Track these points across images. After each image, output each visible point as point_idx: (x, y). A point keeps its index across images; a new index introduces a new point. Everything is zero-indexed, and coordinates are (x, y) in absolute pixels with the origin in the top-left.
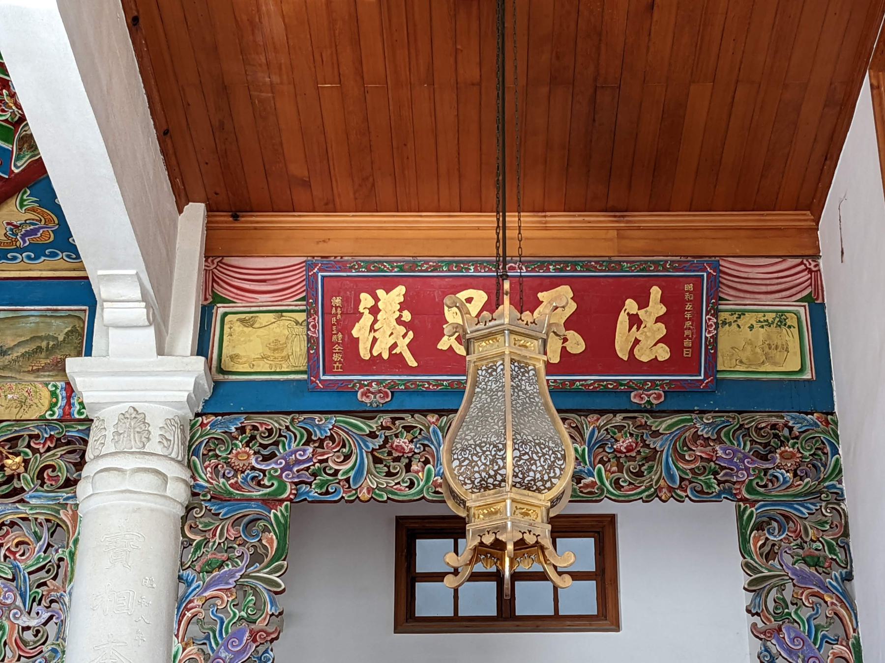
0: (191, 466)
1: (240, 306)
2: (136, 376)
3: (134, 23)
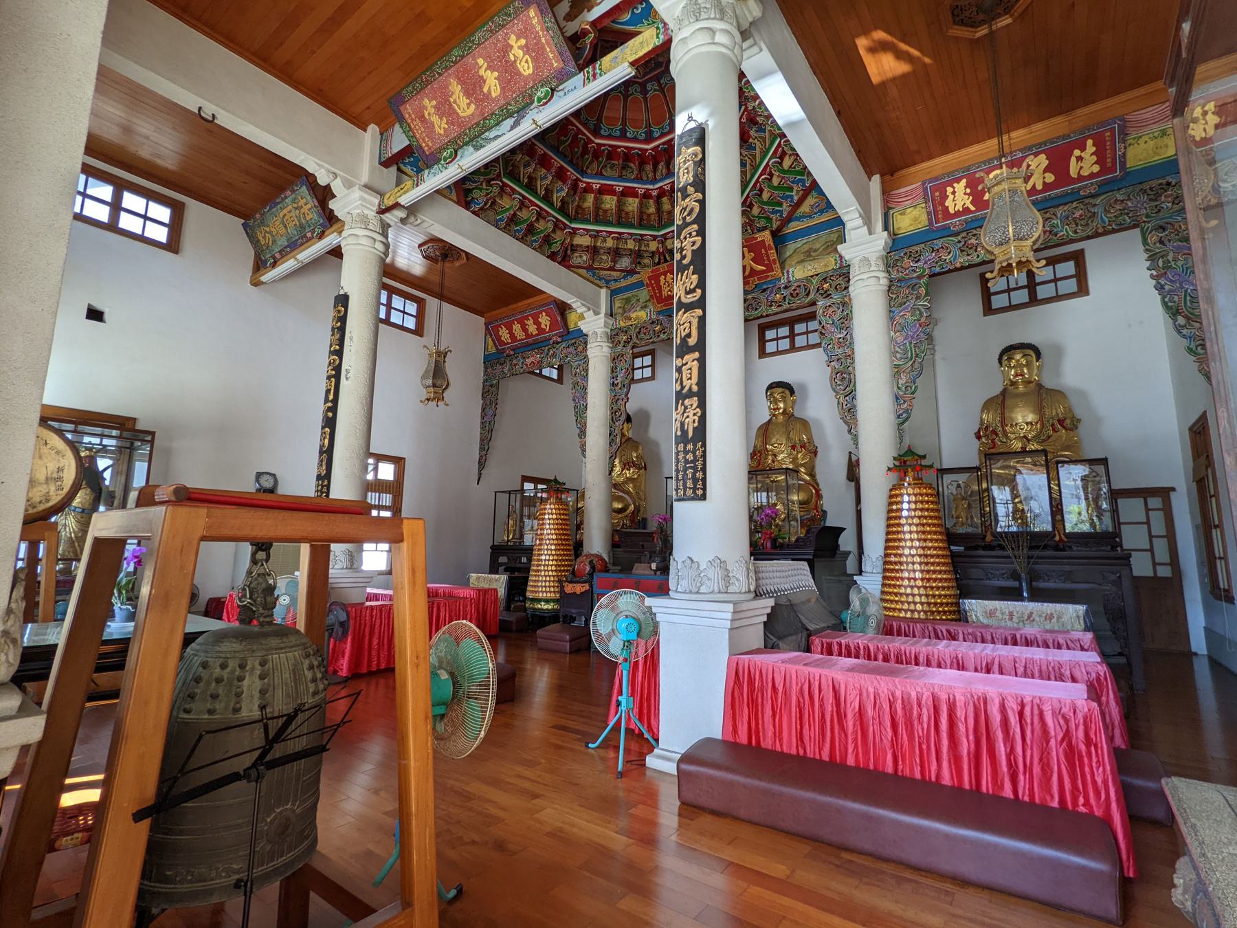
0: (888, 272)
1: (899, 209)
2: (863, 246)
3: (838, 114)
